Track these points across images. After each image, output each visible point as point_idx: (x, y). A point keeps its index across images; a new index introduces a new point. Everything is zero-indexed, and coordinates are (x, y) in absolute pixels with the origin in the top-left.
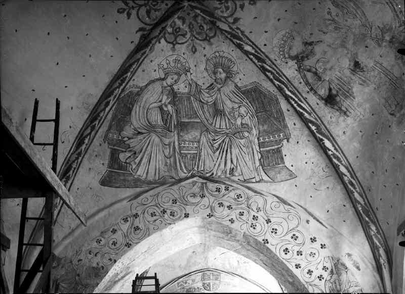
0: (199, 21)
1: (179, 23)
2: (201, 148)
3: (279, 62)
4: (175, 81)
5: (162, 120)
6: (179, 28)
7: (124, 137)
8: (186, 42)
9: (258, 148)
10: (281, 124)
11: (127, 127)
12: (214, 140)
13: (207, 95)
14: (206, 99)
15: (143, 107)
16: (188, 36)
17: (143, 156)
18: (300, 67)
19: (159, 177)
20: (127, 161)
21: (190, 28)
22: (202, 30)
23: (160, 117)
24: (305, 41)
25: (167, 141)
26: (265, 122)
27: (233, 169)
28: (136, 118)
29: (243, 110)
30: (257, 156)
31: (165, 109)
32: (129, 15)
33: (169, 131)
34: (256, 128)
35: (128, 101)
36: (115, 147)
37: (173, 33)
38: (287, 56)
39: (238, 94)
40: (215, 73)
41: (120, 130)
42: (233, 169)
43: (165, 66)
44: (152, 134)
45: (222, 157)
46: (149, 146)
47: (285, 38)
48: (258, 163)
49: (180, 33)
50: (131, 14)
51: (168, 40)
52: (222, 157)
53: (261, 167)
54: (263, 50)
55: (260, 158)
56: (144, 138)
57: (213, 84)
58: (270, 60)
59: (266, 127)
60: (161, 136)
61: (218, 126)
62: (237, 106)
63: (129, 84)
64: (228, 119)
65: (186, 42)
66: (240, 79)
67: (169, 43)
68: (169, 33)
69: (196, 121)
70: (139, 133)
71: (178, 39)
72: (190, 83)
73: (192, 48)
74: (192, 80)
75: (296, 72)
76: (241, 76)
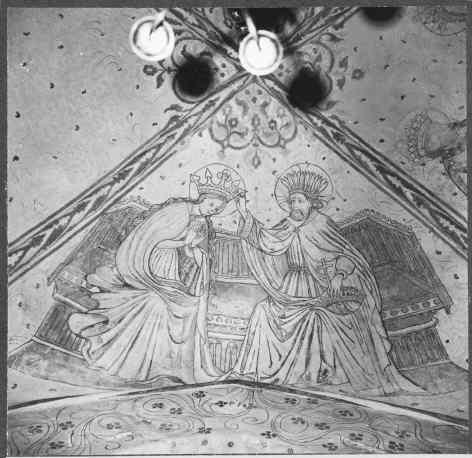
0: (269, 113)
1: (237, 111)
2: (252, 331)
3: (409, 165)
4: (217, 210)
5: (180, 273)
6: (236, 120)
7: (93, 286)
8: (244, 147)
9: (382, 332)
10: (426, 281)
11: (105, 269)
12: (283, 317)
13: (272, 238)
14: (270, 246)
15: (147, 242)
16: (249, 137)
17: (122, 330)
18: (450, 166)
19: (148, 375)
20: (84, 334)
21: (253, 124)
22: (272, 128)
23: (175, 266)
24: (452, 121)
25: (180, 311)
26: (392, 282)
27: (326, 371)
28: (128, 254)
29: (344, 264)
30: (382, 347)
31: (188, 253)
32: (160, 81)
33: (190, 294)
34: (374, 294)
35: (121, 222)
36: (68, 300)
37: (225, 126)
38: (422, 153)
39: (332, 236)
40: (290, 202)
41: (91, 268)
42: (326, 371)
43: (203, 181)
44: (152, 294)
45: (299, 349)
46: (140, 316)
47: (415, 125)
48: (384, 361)
49: (236, 129)
50: (163, 81)
51: (216, 136)
52: (299, 349)
53: (393, 368)
54: (379, 150)
55: (388, 349)
56: (134, 297)
57: (285, 220)
58: (392, 164)
59: (395, 291)
60: (170, 299)
61: (291, 292)
62: (331, 256)
63: (131, 193)
64: (315, 280)
65: (244, 147)
66: (338, 209)
67: (217, 141)
68: (218, 122)
69: (247, 281)
70: (126, 285)
71: (232, 139)
72: (242, 217)
73: (254, 160)
74: (247, 211)
75: (443, 177)
76: (338, 202)
